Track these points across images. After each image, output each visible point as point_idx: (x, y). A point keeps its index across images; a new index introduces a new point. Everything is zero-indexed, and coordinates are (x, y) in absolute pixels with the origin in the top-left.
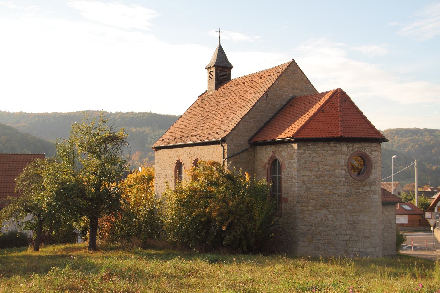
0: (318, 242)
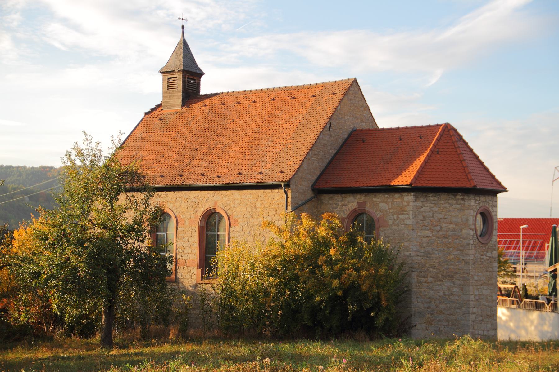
0: (439, 323)
